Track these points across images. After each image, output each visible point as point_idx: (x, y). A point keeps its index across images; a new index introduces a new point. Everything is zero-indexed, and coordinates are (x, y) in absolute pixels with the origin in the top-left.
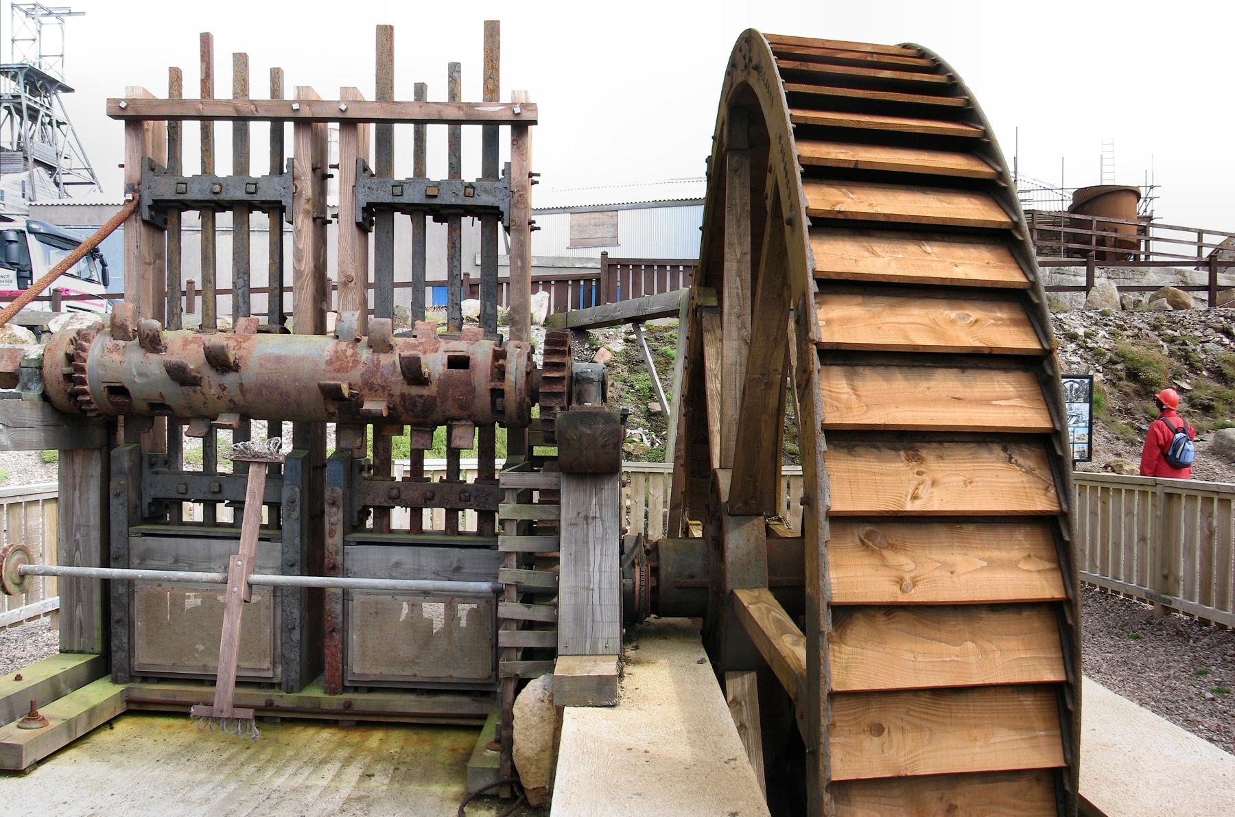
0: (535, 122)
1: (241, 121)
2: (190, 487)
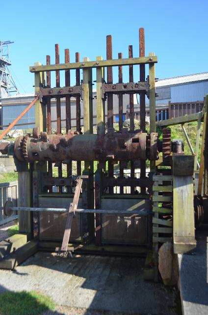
0: (157, 62)
1: (57, 71)
2: (54, 181)
